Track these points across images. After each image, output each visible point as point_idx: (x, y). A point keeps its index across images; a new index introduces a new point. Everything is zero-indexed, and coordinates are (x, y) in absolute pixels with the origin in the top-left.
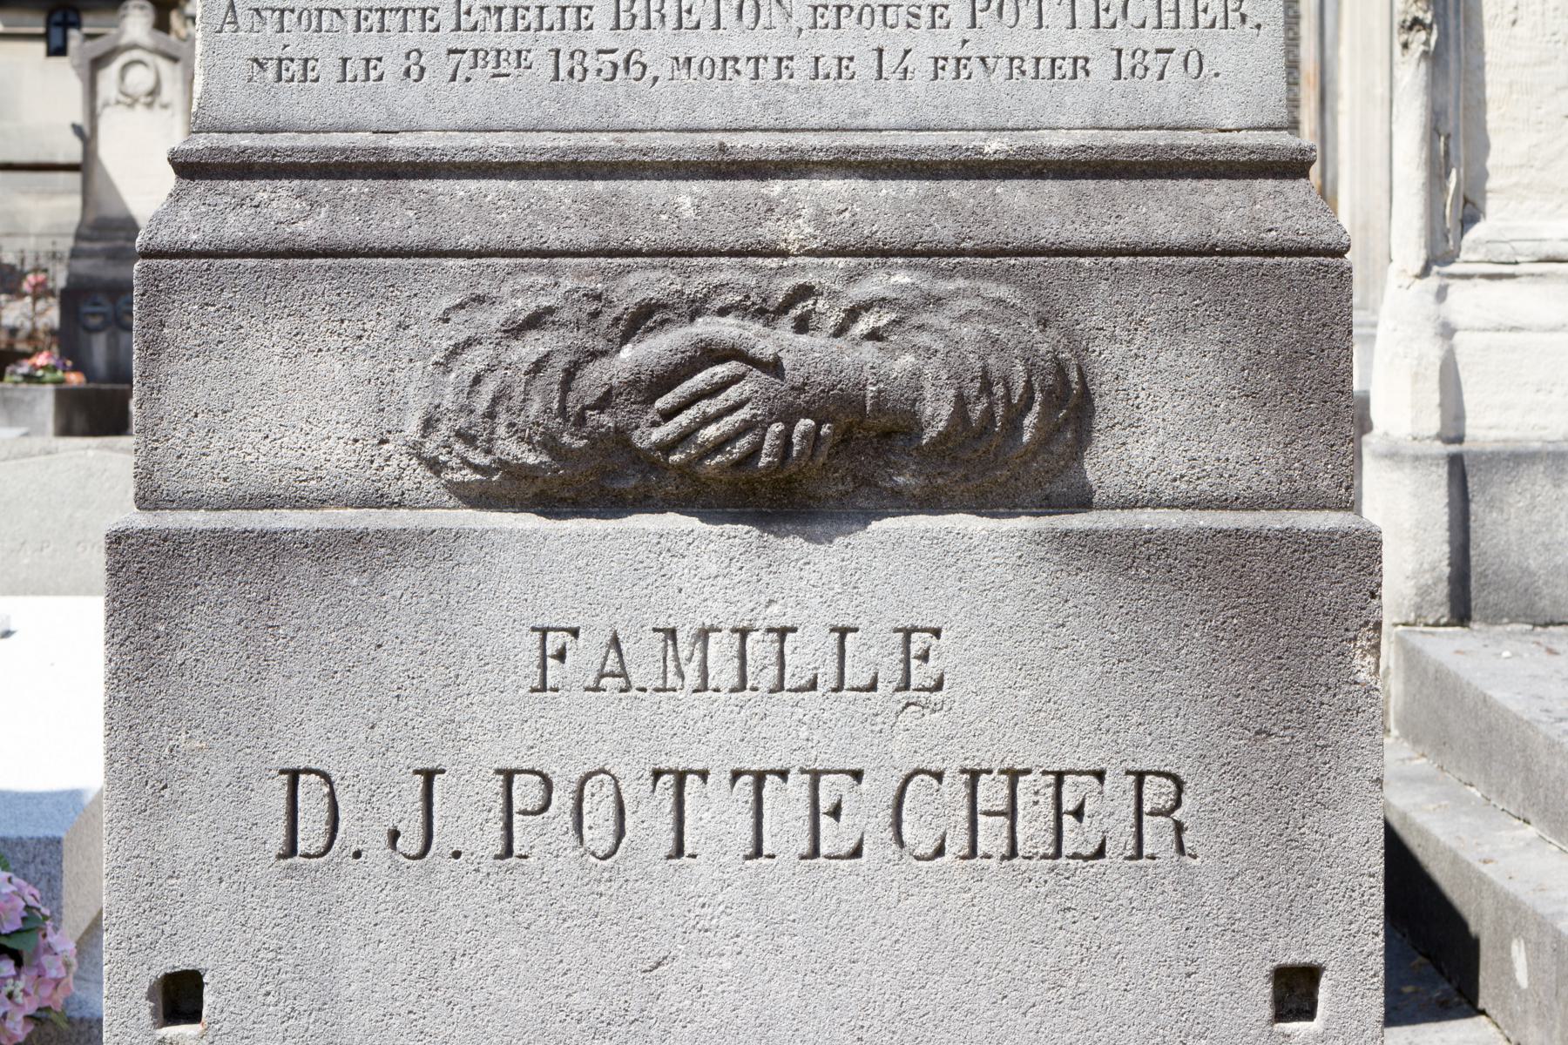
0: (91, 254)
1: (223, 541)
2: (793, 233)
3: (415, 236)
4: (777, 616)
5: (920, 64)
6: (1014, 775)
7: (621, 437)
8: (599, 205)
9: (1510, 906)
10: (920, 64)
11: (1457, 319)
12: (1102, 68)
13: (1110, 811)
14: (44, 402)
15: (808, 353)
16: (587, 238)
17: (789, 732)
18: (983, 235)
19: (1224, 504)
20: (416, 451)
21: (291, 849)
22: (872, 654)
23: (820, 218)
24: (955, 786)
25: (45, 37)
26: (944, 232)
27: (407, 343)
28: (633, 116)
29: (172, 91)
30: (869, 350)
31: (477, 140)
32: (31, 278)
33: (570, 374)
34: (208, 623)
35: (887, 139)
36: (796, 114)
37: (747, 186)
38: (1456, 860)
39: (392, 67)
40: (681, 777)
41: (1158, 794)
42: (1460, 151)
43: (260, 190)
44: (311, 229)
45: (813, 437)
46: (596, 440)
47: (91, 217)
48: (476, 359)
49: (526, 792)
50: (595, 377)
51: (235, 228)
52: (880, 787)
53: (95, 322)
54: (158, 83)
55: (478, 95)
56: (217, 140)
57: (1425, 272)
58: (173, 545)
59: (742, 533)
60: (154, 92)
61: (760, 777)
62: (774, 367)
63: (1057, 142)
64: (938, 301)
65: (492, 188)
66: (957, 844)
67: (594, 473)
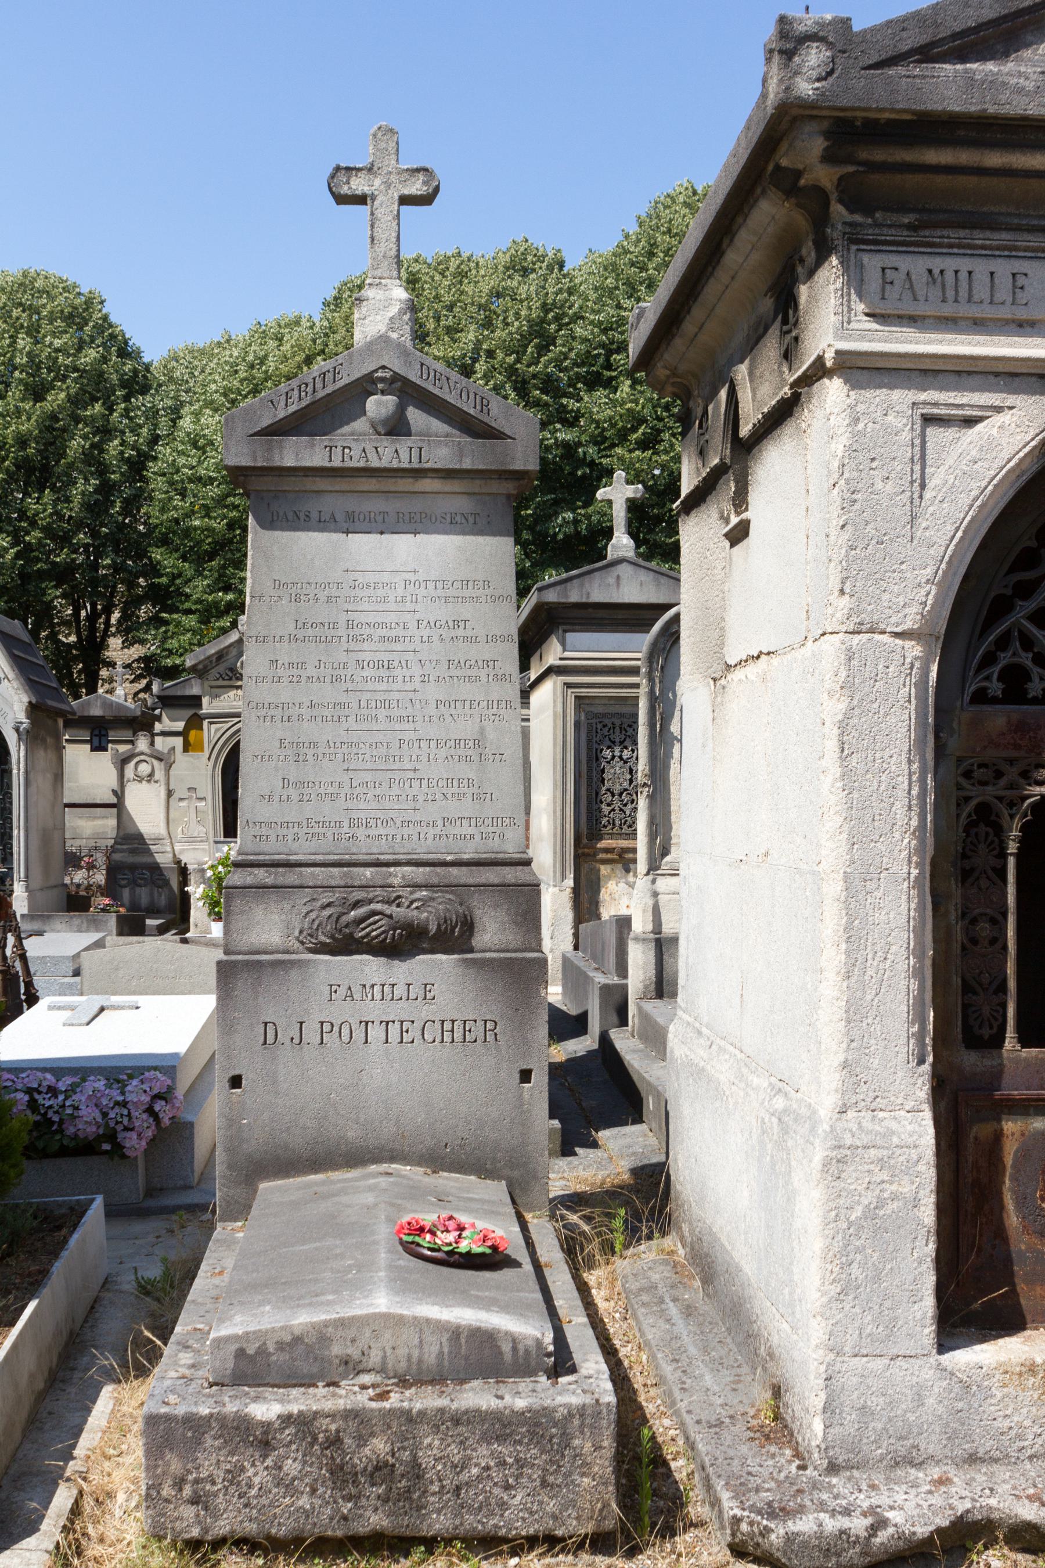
0: (122, 851)
1: (247, 963)
2: (396, 881)
3: (297, 883)
4: (392, 981)
5: (430, 836)
6: (453, 1021)
7: (351, 935)
8: (345, 875)
9: (649, 1084)
10: (430, 836)
11: (659, 890)
12: (478, 837)
13: (478, 1030)
14: (112, 921)
15: (399, 912)
16: (342, 883)
17: (397, 1011)
18: (446, 881)
19: (508, 951)
20: (297, 939)
21: (265, 1043)
22: (416, 991)
23: (403, 878)
24: (438, 1025)
25: (90, 742)
26: (435, 880)
27: (295, 911)
28: (354, 850)
29: (159, 775)
30: (415, 912)
31: (313, 857)
32: (86, 859)
33: (338, 919)
34: (242, 987)
35: (421, 856)
36: (398, 849)
37: (384, 869)
38: (639, 1074)
39: (290, 838)
40: (367, 1023)
41: (490, 1026)
42: (661, 830)
43: (256, 871)
44: (269, 881)
45: (401, 934)
46: (345, 935)
47: (121, 834)
48: (313, 915)
49: (327, 1027)
50: (344, 919)
51: (249, 880)
52: (418, 1025)
53: (124, 882)
54: (153, 770)
55: (313, 845)
56: (244, 857)
57: (648, 874)
58: (234, 963)
59: (383, 959)
60: (151, 775)
61: (387, 1023)
62: (390, 917)
63: (466, 856)
64: (433, 899)
65: (317, 870)
66: (438, 1039)
67: (344, 944)
